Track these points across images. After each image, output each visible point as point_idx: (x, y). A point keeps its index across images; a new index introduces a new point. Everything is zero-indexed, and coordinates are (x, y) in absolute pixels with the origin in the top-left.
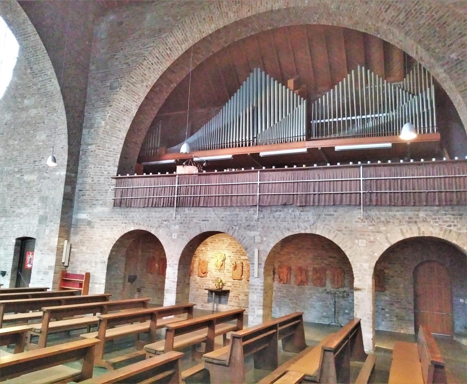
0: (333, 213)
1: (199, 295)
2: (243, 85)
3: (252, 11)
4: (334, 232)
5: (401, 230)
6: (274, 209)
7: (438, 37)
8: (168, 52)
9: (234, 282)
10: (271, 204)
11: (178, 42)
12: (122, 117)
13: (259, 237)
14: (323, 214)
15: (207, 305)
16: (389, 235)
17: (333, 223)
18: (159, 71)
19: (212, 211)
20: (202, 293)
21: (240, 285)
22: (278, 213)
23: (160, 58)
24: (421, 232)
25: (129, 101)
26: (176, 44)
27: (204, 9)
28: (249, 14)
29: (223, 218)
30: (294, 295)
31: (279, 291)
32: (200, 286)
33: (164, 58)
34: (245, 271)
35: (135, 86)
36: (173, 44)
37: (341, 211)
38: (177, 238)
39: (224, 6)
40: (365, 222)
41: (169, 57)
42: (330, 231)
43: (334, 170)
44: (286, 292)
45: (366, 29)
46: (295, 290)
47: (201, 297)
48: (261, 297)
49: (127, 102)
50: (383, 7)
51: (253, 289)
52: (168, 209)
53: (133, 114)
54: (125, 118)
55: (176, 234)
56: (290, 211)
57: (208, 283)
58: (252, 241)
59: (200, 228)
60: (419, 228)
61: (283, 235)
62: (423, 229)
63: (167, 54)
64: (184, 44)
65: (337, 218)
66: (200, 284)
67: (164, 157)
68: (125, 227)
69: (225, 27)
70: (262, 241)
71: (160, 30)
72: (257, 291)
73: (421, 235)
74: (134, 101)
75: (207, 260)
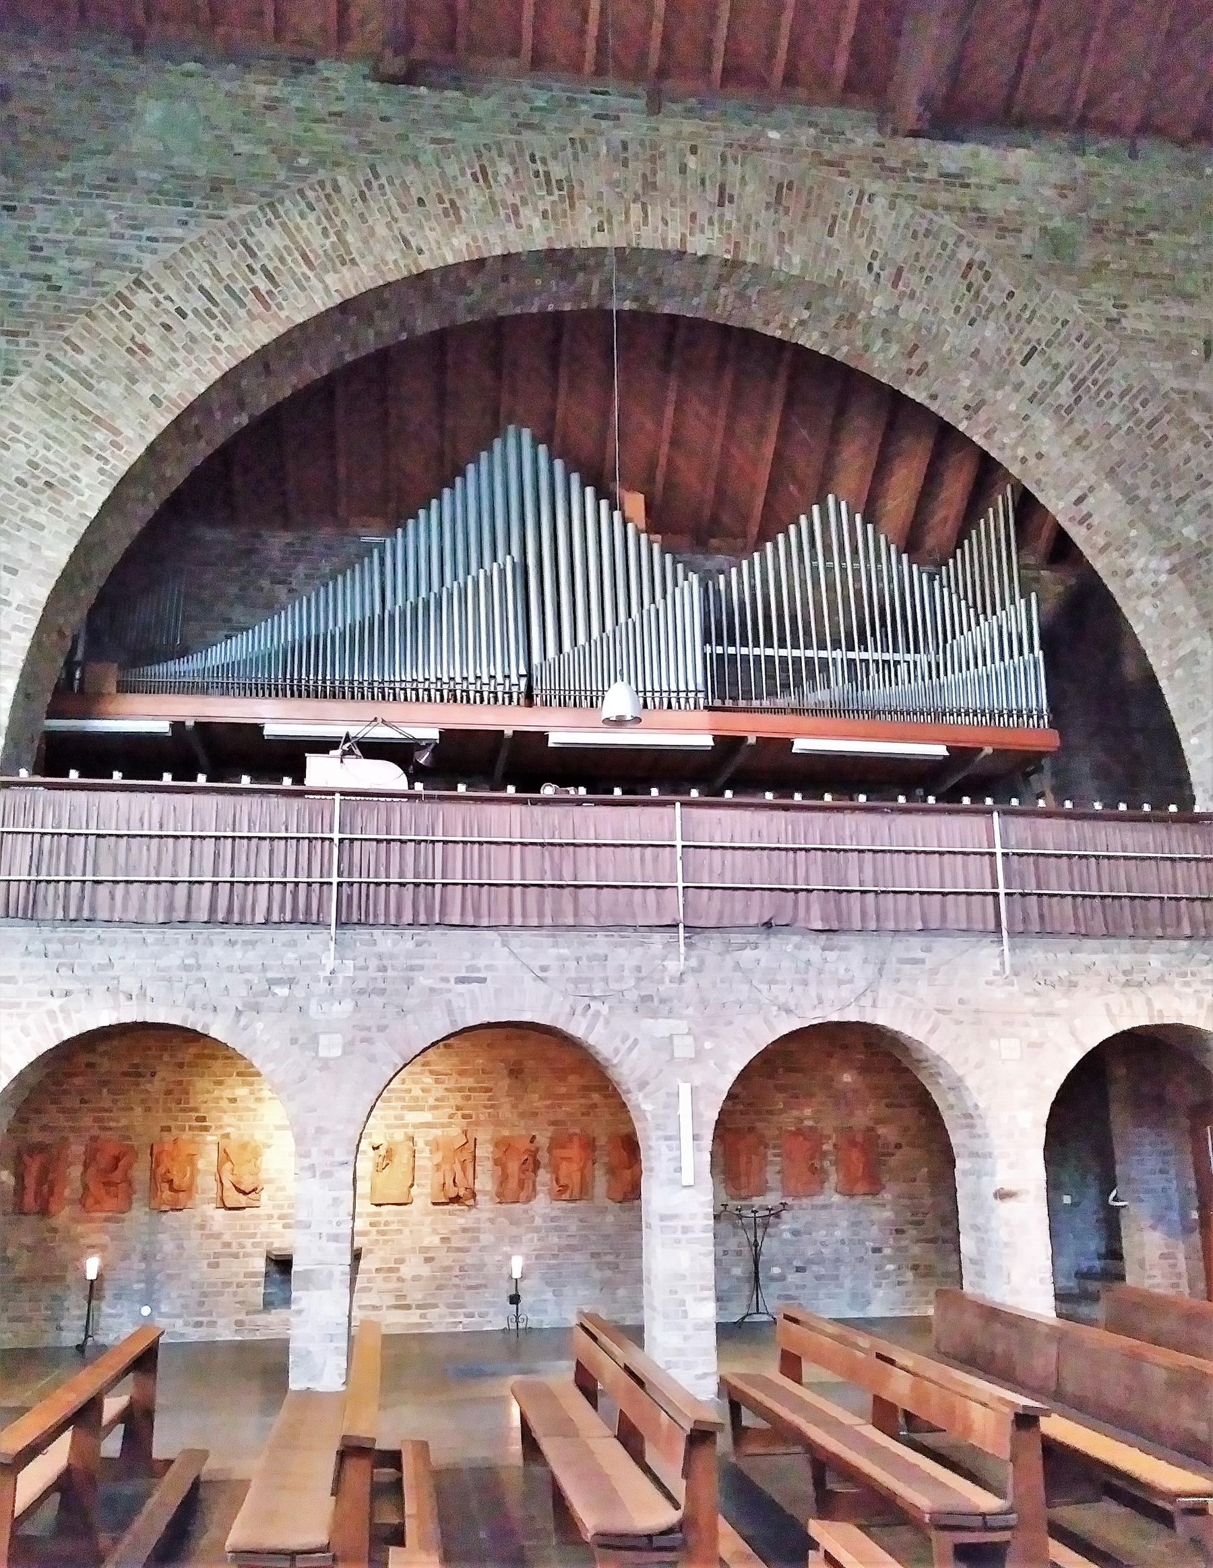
0: (921, 955)
1: (226, 1284)
2: (464, 476)
3: (611, 231)
4: (928, 1017)
5: (1107, 1006)
6: (737, 938)
7: (1153, 473)
8: (263, 285)
9: (379, 1214)
10: (726, 923)
11: (305, 257)
12: (24, 509)
13: (689, 1040)
14: (894, 960)
15: (262, 1319)
16: (1077, 1022)
17: (922, 989)
18: (215, 348)
19: (498, 944)
20: (236, 1275)
21: (404, 1223)
22: (748, 954)
23: (222, 297)
24: (1156, 1013)
25: (61, 443)
26: (295, 261)
27: (418, 165)
28: (602, 240)
29: (544, 969)
30: (607, 1237)
31: (556, 1229)
32: (228, 1245)
33: (242, 304)
34: (423, 1168)
35: (90, 387)
36: (282, 260)
37: (943, 947)
38: (345, 1053)
39: (502, 180)
40: (1013, 985)
41: (267, 307)
42: (915, 1016)
43: (188, 799)
44: (579, 1229)
45: (934, 397)
46: (610, 1218)
47: (234, 1288)
48: (705, 1255)
49: (48, 448)
50: (1016, 347)
51: (675, 1230)
52: (300, 934)
53: (82, 504)
54: (40, 515)
55: (338, 1038)
56: (790, 948)
57: (264, 1228)
58: (665, 1056)
59: (450, 1012)
60: (1149, 1002)
61: (771, 1028)
62: (1157, 1005)
63: (255, 290)
64: (336, 271)
65: (934, 971)
66: (227, 1237)
67: (111, 708)
68: (63, 1009)
69: (506, 258)
70: (698, 1052)
71: (216, 187)
72: (690, 1235)
73: (1157, 1021)
74: (88, 450)
75: (259, 1137)
